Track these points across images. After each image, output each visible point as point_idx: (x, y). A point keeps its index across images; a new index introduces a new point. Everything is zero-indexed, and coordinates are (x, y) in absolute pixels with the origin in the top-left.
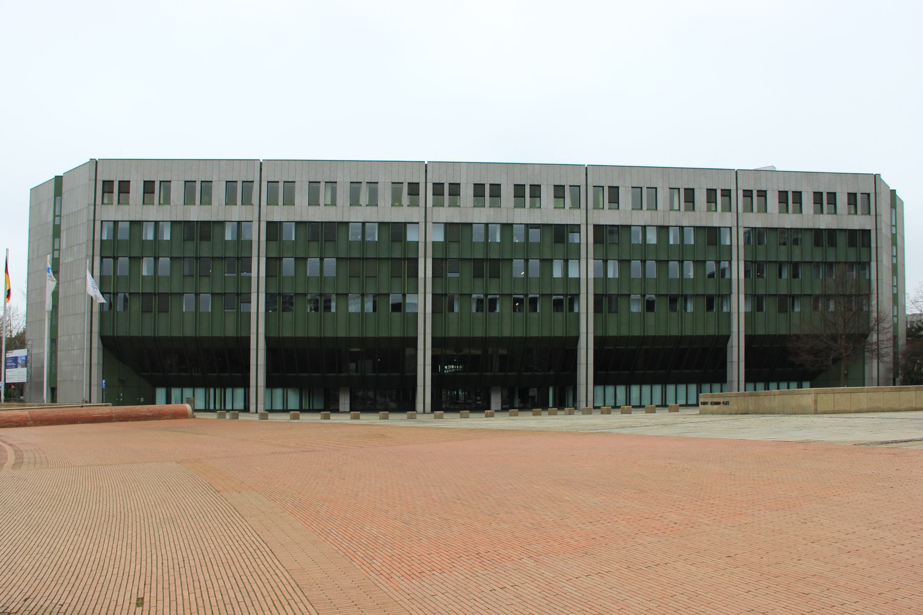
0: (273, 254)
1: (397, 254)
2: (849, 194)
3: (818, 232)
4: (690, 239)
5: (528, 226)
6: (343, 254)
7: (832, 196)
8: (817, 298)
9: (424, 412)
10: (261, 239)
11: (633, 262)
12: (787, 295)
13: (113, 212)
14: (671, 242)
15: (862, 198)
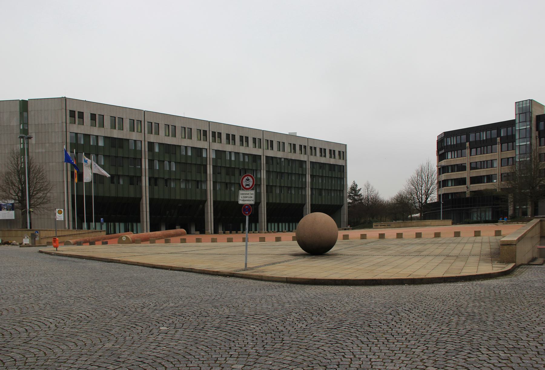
0: (151, 158)
1: (199, 163)
2: (300, 145)
3: (330, 165)
4: (101, 143)
5: (244, 154)
6: (178, 161)
7: (81, 115)
8: (227, 184)
9: (211, 234)
10: (146, 150)
11: (165, 162)
12: (134, 176)
13: (76, 128)
14: (92, 144)
15: (155, 126)
